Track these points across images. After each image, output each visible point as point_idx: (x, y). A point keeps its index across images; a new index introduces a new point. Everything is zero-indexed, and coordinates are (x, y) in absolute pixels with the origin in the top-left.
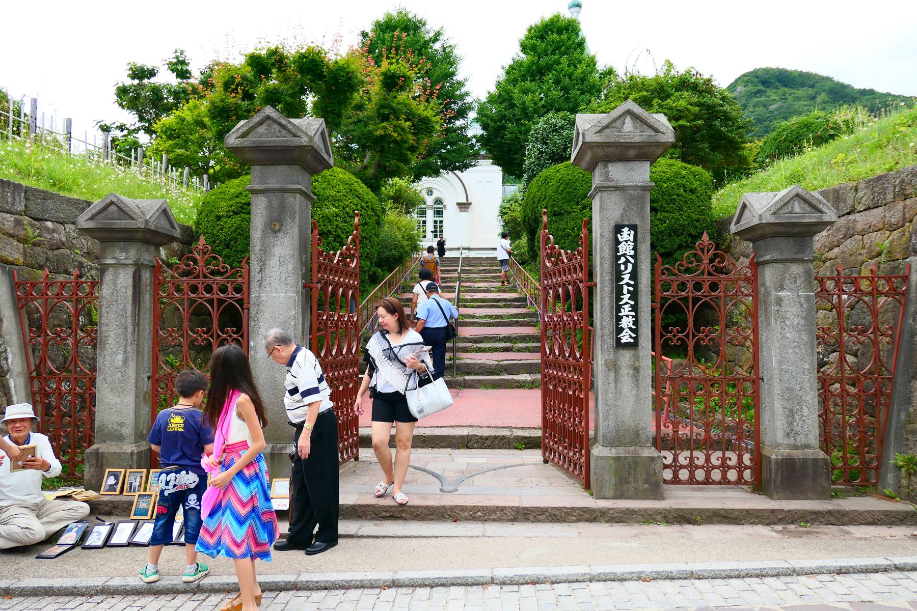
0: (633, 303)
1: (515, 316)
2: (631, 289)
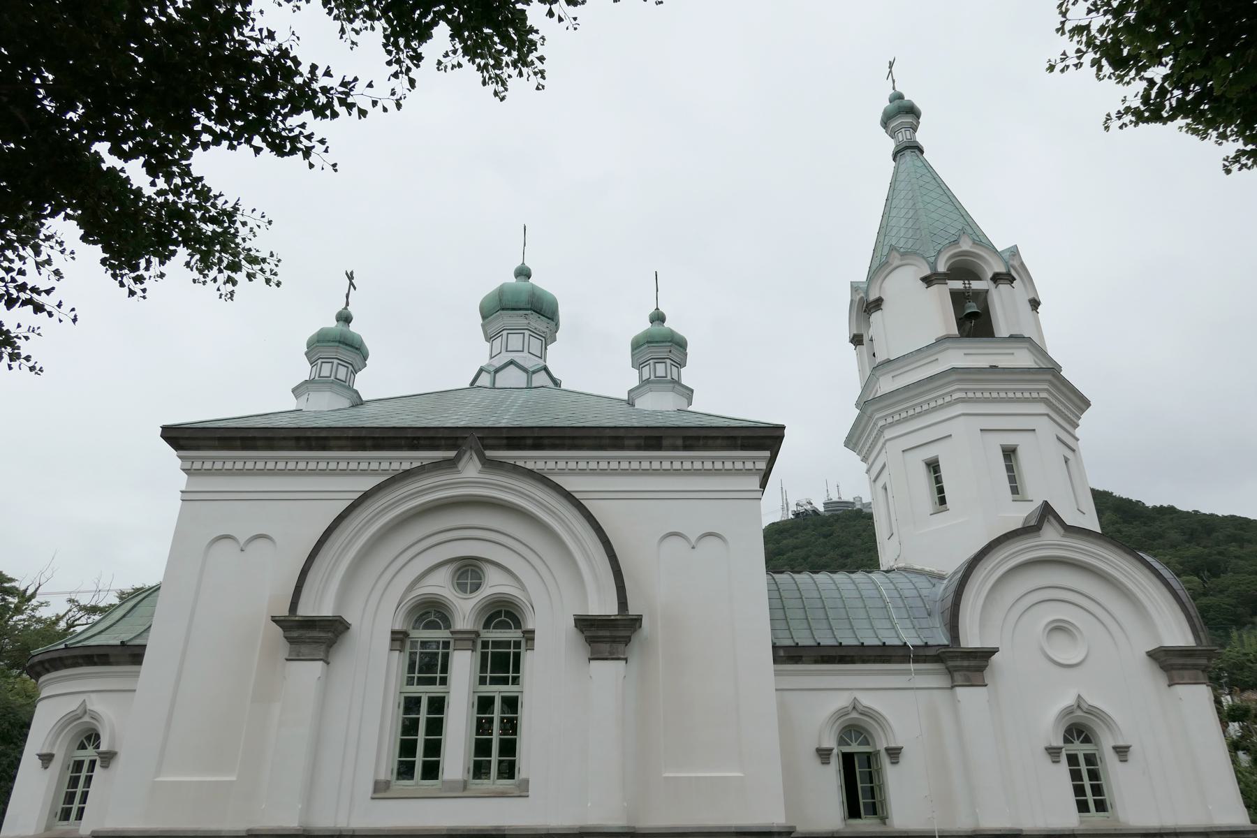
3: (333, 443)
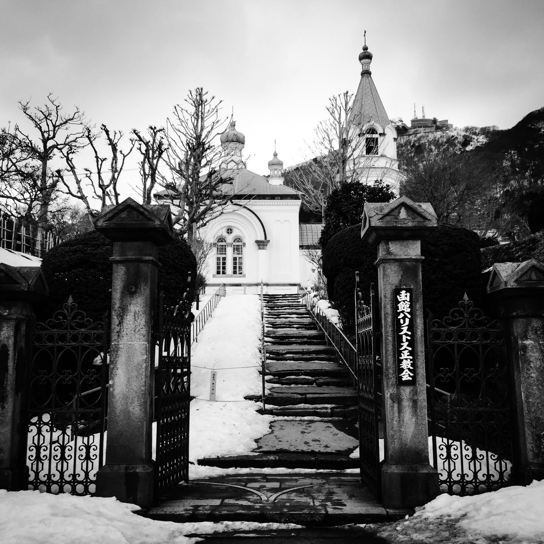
0: (410, 349)
2: (409, 338)
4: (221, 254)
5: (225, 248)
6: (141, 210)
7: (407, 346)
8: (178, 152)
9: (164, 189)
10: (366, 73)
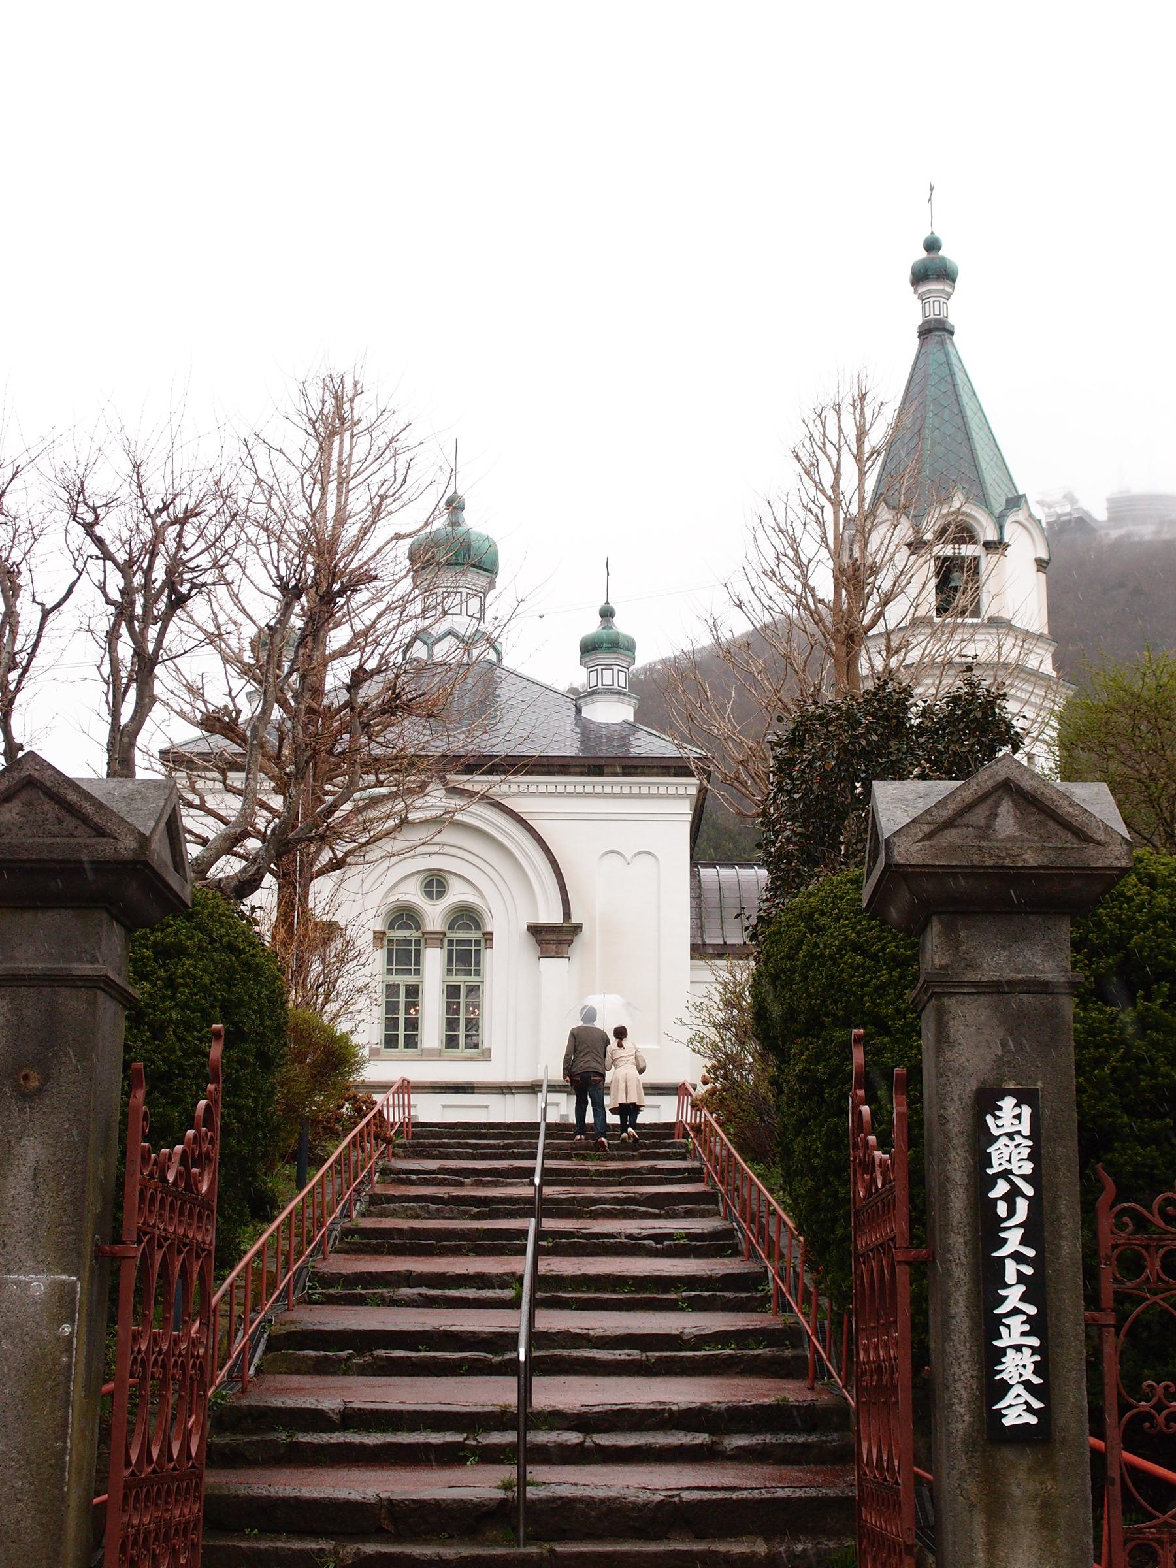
0: (1032, 1310)
1: (740, 1337)
2: (1028, 1270)
3: (646, 771)
4: (398, 972)
5: (418, 952)
6: (72, 797)
7: (1022, 1299)
8: (251, 598)
9: (196, 732)
10: (934, 331)
